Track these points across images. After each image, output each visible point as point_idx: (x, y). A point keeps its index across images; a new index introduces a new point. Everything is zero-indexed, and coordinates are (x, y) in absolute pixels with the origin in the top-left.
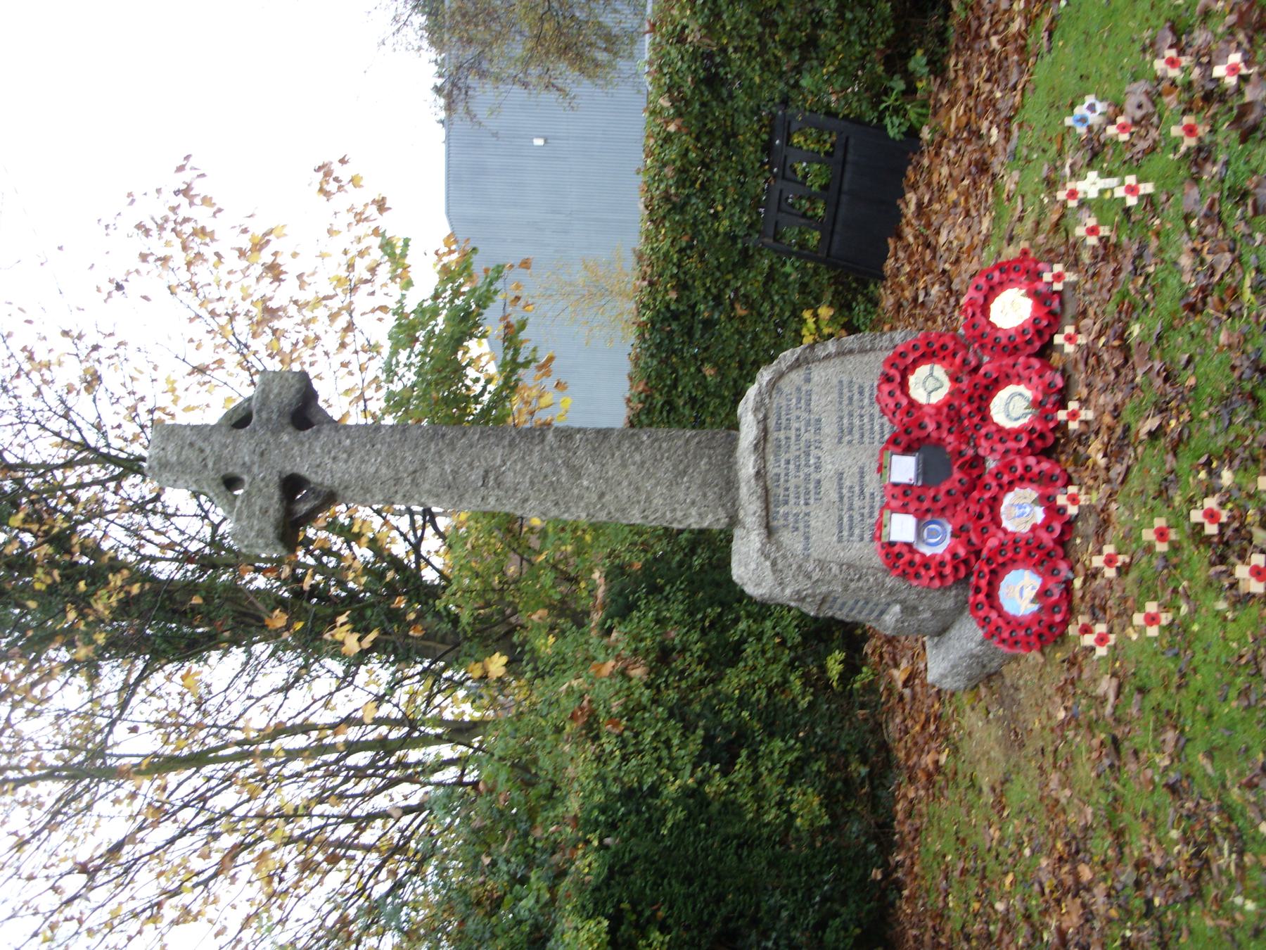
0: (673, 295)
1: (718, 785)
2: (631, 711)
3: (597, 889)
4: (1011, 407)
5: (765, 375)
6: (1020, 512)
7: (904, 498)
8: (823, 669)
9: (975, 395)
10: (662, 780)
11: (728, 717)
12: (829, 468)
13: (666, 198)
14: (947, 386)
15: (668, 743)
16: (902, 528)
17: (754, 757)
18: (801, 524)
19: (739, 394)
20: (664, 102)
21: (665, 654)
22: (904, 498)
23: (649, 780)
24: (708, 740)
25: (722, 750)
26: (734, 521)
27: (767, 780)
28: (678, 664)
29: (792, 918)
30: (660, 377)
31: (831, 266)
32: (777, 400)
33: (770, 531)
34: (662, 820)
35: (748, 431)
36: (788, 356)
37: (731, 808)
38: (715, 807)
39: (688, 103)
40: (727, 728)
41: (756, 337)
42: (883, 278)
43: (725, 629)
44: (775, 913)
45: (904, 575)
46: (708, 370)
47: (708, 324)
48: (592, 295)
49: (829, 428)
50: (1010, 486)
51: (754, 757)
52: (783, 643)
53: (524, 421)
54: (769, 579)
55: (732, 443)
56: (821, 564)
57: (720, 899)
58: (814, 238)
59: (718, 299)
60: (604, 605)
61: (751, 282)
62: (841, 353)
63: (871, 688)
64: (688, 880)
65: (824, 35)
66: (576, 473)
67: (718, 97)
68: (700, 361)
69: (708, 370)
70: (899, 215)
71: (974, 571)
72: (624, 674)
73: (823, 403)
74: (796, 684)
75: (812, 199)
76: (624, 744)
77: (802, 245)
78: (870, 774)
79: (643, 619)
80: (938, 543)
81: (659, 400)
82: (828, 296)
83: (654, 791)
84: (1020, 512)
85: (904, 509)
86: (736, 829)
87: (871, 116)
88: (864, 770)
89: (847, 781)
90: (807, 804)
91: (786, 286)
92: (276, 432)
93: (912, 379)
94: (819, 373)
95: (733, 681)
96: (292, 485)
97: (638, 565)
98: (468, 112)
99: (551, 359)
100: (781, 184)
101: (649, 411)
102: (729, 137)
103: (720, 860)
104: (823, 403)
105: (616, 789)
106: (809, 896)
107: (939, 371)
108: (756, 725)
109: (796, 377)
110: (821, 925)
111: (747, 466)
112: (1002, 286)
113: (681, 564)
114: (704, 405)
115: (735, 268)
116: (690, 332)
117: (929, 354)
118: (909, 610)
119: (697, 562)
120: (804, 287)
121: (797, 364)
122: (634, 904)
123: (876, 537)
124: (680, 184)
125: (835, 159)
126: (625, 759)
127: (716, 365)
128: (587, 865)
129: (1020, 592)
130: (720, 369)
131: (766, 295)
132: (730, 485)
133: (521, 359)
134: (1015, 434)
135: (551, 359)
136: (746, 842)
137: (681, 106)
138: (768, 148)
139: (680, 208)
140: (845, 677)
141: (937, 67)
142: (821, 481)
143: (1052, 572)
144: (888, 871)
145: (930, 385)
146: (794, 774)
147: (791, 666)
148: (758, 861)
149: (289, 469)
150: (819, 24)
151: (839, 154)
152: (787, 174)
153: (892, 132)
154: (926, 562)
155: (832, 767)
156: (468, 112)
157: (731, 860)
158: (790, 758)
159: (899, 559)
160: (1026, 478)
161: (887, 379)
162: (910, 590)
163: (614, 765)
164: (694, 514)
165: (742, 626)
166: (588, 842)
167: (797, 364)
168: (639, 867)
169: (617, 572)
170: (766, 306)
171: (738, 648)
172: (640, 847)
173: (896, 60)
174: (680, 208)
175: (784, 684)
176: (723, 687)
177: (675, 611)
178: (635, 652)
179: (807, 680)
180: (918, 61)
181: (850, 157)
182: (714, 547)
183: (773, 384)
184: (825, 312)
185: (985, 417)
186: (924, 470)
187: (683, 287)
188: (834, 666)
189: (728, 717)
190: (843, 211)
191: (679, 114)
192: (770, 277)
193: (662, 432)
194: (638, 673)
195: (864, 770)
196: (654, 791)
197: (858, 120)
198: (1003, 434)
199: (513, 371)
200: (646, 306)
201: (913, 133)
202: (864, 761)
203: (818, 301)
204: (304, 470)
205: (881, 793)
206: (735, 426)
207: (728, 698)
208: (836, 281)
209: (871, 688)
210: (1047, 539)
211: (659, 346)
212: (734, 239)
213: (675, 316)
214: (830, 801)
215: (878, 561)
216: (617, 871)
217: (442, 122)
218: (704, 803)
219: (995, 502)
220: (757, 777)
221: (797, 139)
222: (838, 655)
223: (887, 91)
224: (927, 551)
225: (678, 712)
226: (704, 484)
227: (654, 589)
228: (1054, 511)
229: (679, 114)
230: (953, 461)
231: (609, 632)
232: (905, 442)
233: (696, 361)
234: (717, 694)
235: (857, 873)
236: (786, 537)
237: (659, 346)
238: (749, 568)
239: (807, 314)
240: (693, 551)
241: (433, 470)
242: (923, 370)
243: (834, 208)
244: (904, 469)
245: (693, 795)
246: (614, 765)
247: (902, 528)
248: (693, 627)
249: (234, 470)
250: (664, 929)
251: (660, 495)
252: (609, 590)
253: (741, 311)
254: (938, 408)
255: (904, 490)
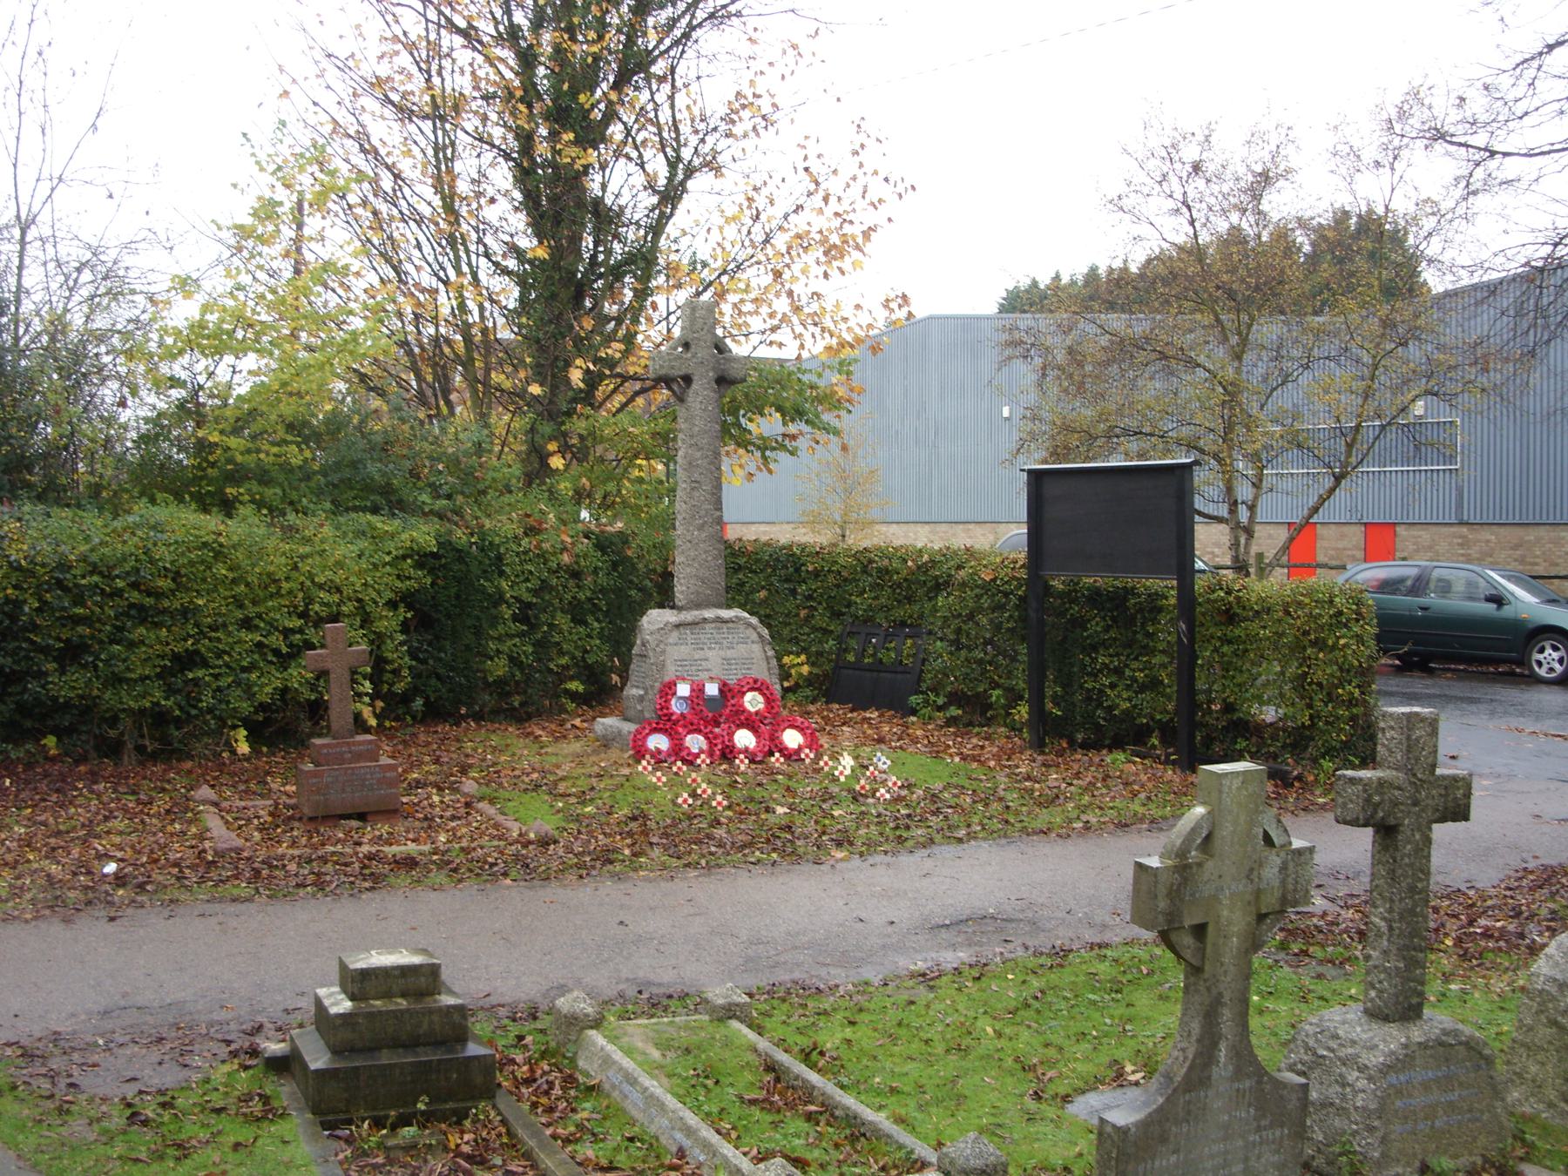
0: (810, 568)
1: (508, 614)
2: (543, 556)
3: (451, 543)
4: (744, 738)
5: (754, 620)
6: (695, 742)
7: (698, 690)
8: (572, 678)
9: (751, 723)
10: (507, 578)
11: (543, 617)
12: (710, 654)
13: (871, 561)
14: (752, 710)
15: (527, 580)
16: (683, 690)
17: (522, 635)
18: (682, 641)
19: (742, 606)
20: (926, 558)
21: (576, 575)
22: (698, 690)
23: (508, 570)
24: (529, 605)
25: (525, 614)
26: (680, 609)
27: (509, 643)
28: (571, 583)
29: (440, 659)
30: (757, 561)
31: (834, 670)
32: (742, 628)
33: (678, 626)
34: (487, 579)
35: (726, 614)
36: (765, 632)
37: (495, 620)
38: (493, 611)
39: (925, 573)
40: (536, 617)
41: (787, 624)
42: (827, 703)
43: (593, 613)
44: (441, 650)
45: (661, 691)
46: (763, 594)
47: (794, 592)
48: (844, 479)
49: (730, 654)
50: (707, 738)
51: (522, 635)
52: (586, 651)
53: (723, 450)
54: (653, 628)
55: (720, 606)
56: (663, 652)
57: (449, 616)
58: (851, 658)
59: (810, 598)
60: (603, 532)
61: (821, 620)
62: (767, 658)
63: (563, 710)
64: (458, 597)
65: (963, 653)
66: (701, 528)
67: (929, 590)
68: (769, 587)
69: (763, 594)
70: (865, 710)
71: (666, 723)
72: (564, 549)
73: (741, 650)
74: (564, 661)
75: (874, 655)
76: (526, 553)
77: (846, 651)
78: (515, 709)
79: (597, 560)
80: (677, 707)
81: (742, 561)
82: (815, 671)
83: (502, 573)
84: (695, 742)
85: (692, 690)
86: (485, 626)
87: (924, 686)
88: (516, 704)
89: (509, 694)
90: (499, 668)
91: (820, 642)
92: (713, 369)
93: (756, 693)
94: (757, 648)
95: (563, 620)
96: (688, 379)
97: (629, 553)
98: (1010, 358)
99: (770, 472)
100: (883, 634)
101: (733, 555)
102: (910, 599)
103: (469, 615)
104: (741, 650)
105: (502, 550)
106: (452, 669)
107: (761, 706)
108: (539, 636)
109: (754, 636)
110: (439, 677)
111: (709, 614)
112: (804, 735)
113: (631, 582)
114: (739, 592)
115: (829, 608)
116: (787, 580)
117: (769, 701)
118: (641, 699)
119: (633, 593)
120: (820, 654)
121: (761, 636)
122: (444, 566)
123: (678, 678)
124: (879, 570)
125: (898, 667)
126: (518, 554)
127: (767, 598)
128: (460, 536)
129: (658, 742)
130: (764, 602)
131: (815, 629)
132: (698, 606)
133: (768, 453)
134: (731, 740)
135: (770, 472)
136: (478, 632)
137: (923, 569)
138: (903, 624)
139: (865, 571)
140: (567, 691)
141: (951, 721)
142: (700, 648)
143: (669, 755)
144: (464, 718)
145: (753, 702)
146: (514, 660)
147: (574, 657)
148: (469, 638)
149: (695, 378)
150: (970, 650)
151: (900, 669)
152: (888, 637)
153: (913, 698)
154: (668, 701)
155: (517, 683)
156: (1010, 358)
157: (469, 622)
158: (523, 658)
159: (668, 689)
160: (711, 744)
161: (755, 681)
162: (653, 695)
163: (514, 547)
164: (680, 590)
165: (596, 624)
166: (472, 535)
167: (761, 636)
168: (463, 568)
169: (624, 538)
170: (807, 630)
171: (584, 623)
172: (475, 570)
173: (955, 698)
174: (865, 571)
175: (562, 653)
176: (559, 614)
177: (602, 579)
178: (577, 556)
179: (566, 667)
180: (954, 711)
181: (899, 676)
182: (665, 599)
183: (750, 625)
184: (805, 669)
185: (739, 726)
186: (712, 699)
187: (816, 574)
188: (574, 686)
189: (543, 617)
190: (868, 674)
191: (919, 568)
192: (826, 632)
193: (723, 570)
194: (566, 558)
195: (516, 704)
196: (502, 573)
197: (920, 680)
198: (731, 735)
199: (759, 448)
200: (803, 550)
201: (914, 712)
202: (522, 704)
203: (813, 664)
204: (695, 386)
205: (502, 717)
206: (729, 607)
207: (553, 617)
208: (826, 675)
209: (563, 710)
210: (684, 753)
211: (777, 560)
212: (849, 606)
213: (797, 570)
214: (501, 682)
215: (667, 679)
216: (460, 554)
217: (1057, 278)
218: (496, 604)
219: (699, 731)
220: (512, 636)
221: (909, 642)
222: (581, 688)
223: (937, 695)
224: (673, 702)
225: (544, 586)
226: (698, 593)
227: (615, 565)
228: (697, 756)
229: (919, 568)
230: (716, 714)
231: (587, 537)
232: (725, 689)
233: (769, 582)
234: (555, 610)
235: (464, 698)
236: (675, 634)
237: (777, 560)
238: (655, 619)
239: (803, 657)
240: (640, 590)
241: (699, 454)
242: (760, 699)
243: (870, 668)
244: (712, 690)
245: (499, 599)
246: (514, 547)
247: (683, 690)
248: (594, 592)
249: (693, 349)
250: (433, 584)
251: (692, 568)
252: (612, 534)
253: (803, 613)
254: (742, 705)
255: (701, 690)
